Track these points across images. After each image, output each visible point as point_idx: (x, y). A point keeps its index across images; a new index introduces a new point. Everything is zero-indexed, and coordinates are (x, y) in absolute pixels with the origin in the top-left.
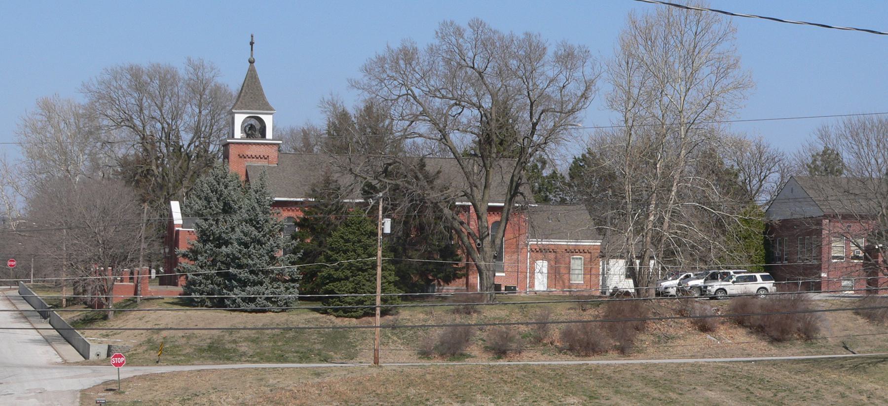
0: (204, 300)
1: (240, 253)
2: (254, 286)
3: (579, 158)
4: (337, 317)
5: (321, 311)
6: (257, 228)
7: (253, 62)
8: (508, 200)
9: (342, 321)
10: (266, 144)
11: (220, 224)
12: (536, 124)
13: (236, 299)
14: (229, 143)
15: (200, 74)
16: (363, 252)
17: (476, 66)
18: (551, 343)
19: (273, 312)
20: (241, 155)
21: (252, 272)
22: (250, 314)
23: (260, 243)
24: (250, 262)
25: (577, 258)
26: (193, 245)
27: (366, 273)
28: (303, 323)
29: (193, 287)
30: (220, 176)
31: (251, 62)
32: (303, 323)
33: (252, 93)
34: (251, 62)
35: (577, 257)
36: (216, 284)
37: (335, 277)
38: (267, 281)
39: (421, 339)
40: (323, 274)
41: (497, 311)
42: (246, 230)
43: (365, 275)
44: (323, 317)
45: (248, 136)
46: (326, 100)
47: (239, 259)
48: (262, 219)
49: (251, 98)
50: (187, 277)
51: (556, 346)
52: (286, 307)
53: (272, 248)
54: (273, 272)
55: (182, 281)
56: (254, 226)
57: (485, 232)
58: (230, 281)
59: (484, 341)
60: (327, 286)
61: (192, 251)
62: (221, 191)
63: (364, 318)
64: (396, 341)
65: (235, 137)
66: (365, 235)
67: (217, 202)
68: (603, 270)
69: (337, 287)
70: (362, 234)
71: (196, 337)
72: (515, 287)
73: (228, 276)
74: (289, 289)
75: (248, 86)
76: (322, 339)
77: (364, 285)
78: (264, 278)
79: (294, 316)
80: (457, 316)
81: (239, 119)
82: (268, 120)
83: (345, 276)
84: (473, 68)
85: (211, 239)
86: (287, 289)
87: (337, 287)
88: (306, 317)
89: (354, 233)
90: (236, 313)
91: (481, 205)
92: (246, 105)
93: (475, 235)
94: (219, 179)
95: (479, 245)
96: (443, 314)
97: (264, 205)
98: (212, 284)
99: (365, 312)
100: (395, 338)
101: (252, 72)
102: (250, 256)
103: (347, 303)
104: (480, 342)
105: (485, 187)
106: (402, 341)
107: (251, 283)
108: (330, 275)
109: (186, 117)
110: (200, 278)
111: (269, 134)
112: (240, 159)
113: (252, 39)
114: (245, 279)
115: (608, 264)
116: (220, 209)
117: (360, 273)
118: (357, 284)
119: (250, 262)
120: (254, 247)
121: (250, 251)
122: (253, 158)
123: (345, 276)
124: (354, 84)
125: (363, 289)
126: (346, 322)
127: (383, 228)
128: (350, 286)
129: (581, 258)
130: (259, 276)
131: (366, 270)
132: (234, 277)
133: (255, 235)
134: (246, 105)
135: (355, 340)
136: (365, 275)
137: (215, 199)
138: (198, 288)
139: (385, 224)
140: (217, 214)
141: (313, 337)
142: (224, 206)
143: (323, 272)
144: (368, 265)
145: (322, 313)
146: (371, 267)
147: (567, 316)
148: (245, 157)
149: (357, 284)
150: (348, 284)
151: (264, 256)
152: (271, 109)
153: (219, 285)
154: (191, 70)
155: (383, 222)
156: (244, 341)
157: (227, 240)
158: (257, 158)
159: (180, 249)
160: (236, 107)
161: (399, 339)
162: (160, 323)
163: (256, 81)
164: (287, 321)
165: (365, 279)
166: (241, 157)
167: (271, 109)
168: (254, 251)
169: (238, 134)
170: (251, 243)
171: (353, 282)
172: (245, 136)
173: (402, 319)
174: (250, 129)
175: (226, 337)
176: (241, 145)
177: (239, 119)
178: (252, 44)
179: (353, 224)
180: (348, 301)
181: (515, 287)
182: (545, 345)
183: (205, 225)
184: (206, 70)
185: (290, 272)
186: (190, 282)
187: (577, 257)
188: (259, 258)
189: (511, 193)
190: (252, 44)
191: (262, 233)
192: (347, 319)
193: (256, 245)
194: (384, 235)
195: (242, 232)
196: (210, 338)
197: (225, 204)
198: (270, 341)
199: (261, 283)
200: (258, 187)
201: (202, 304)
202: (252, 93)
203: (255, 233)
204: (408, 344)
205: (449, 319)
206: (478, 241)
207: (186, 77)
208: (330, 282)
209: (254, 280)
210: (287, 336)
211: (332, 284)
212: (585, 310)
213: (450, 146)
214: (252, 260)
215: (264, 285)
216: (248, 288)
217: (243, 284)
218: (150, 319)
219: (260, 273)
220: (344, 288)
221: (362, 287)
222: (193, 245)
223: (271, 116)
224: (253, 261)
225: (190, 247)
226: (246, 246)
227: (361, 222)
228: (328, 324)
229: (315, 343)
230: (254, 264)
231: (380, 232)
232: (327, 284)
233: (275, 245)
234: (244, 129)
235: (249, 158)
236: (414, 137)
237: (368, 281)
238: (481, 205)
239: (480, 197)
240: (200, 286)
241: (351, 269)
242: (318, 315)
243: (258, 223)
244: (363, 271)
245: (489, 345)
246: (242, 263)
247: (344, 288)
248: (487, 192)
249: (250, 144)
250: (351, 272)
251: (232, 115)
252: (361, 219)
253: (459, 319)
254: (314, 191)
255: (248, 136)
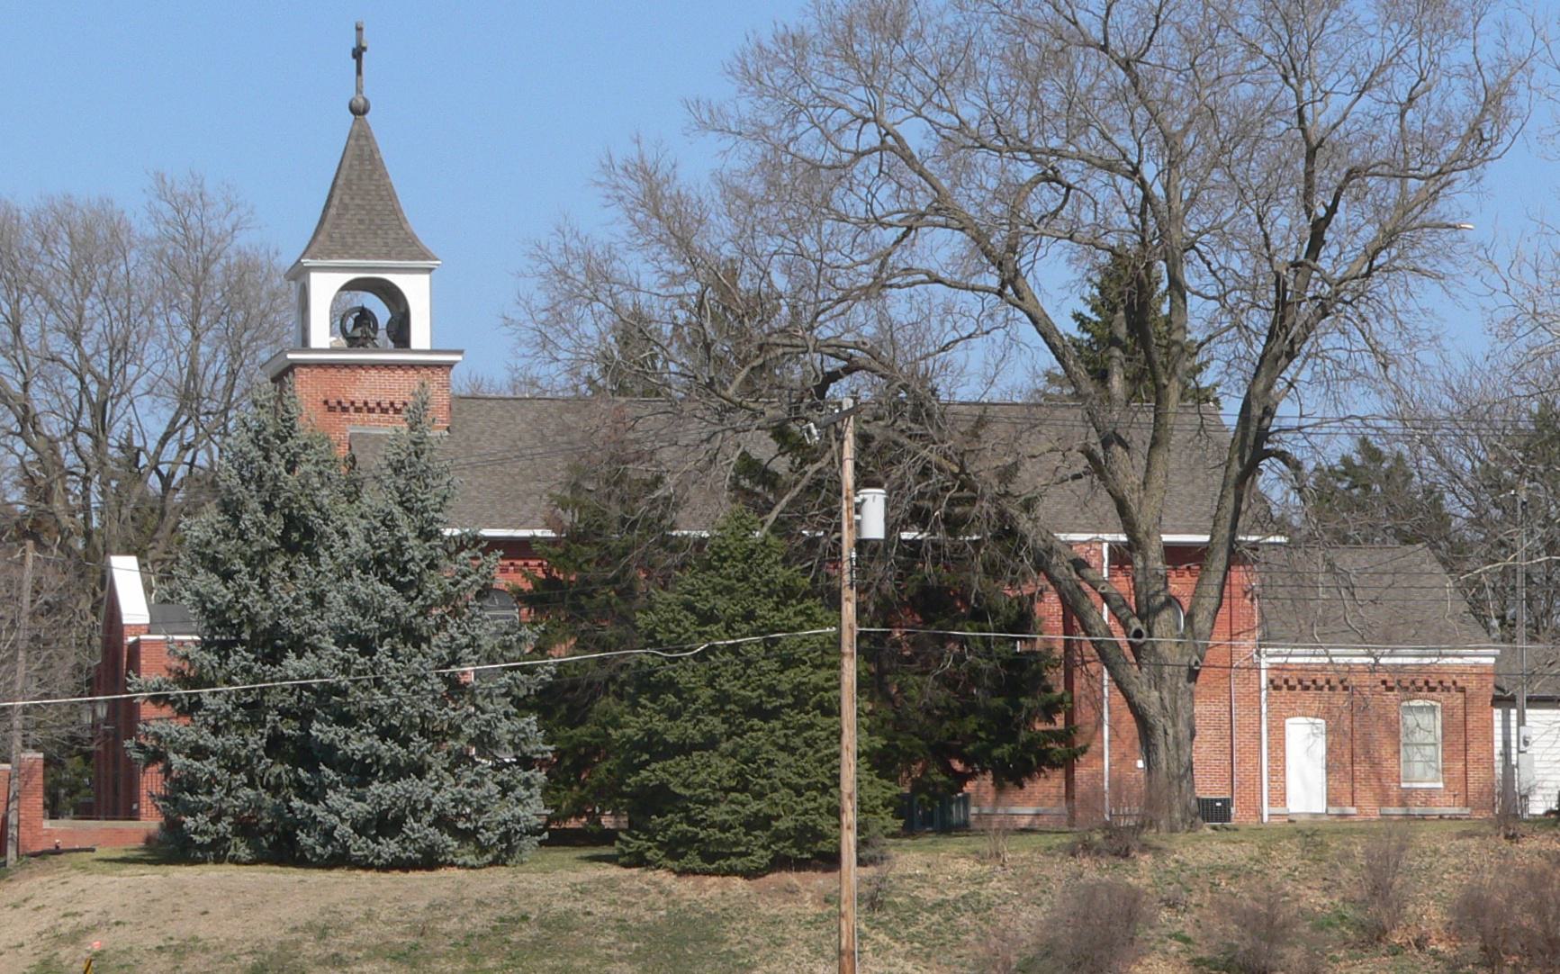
0: (225, 839)
1: (345, 672)
2: (395, 780)
3: (1331, 469)
4: (682, 873)
5: (621, 860)
6: (401, 588)
7: (365, 112)
8: (1231, 482)
9: (696, 886)
10: (413, 366)
11: (275, 584)
12: (1327, 220)
13: (335, 827)
14: (292, 366)
15: (193, 220)
16: (762, 650)
17: (1114, 42)
18: (1418, 946)
19: (464, 866)
20: (333, 402)
21: (385, 733)
22: (384, 875)
23: (414, 637)
24: (381, 699)
25: (1421, 708)
26: (186, 657)
27: (776, 724)
28: (565, 897)
29: (188, 797)
30: (271, 430)
31: (358, 111)
32: (565, 897)
33: (362, 207)
34: (358, 111)
35: (1421, 703)
36: (267, 787)
37: (670, 738)
38: (438, 761)
39: (971, 937)
40: (629, 731)
41: (1218, 846)
42: (362, 591)
43: (773, 731)
44: (632, 877)
45: (353, 342)
46: (618, 161)
47: (343, 693)
48: (418, 556)
49: (361, 222)
50: (168, 770)
51: (1435, 953)
52: (504, 851)
53: (453, 653)
54: (459, 729)
55: (151, 782)
56: (392, 582)
57: (1157, 593)
58: (313, 769)
59: (1187, 940)
60: (644, 773)
61: (183, 679)
62: (276, 477)
63: (770, 876)
64: (887, 948)
65: (314, 344)
66: (769, 595)
67: (261, 515)
68: (1506, 743)
69: (677, 774)
70: (757, 592)
71: (205, 950)
72: (1227, 803)
73: (308, 754)
74: (513, 789)
75: (349, 183)
76: (634, 945)
77: (770, 763)
78: (429, 752)
79: (533, 877)
80: (1086, 862)
81: (325, 288)
82: (415, 289)
83: (703, 734)
84: (1105, 48)
85: (246, 636)
86: (505, 789)
87: (677, 774)
88: (572, 877)
89: (730, 590)
90: (336, 874)
91: (1140, 503)
92: (344, 245)
93: (1125, 604)
94: (266, 441)
95: (1138, 634)
96: (1037, 857)
97: (425, 510)
98: (251, 784)
99: (776, 853)
100: (882, 938)
101: (363, 142)
102: (378, 683)
103: (712, 825)
104: (1175, 946)
105: (1155, 443)
106: (908, 946)
107: (386, 769)
108: (651, 733)
109: (151, 352)
110: (209, 766)
111: (420, 335)
112: (331, 417)
113: (359, 39)
114: (365, 757)
115: (1521, 721)
116: (273, 537)
117: (756, 722)
118: (746, 761)
119: (381, 699)
120: (393, 649)
121: (379, 663)
122: (371, 410)
123: (703, 734)
124: (706, 116)
125: (766, 777)
126: (709, 891)
127: (858, 523)
128: (724, 767)
129: (1433, 708)
130: (412, 745)
131: (775, 713)
132: (328, 753)
133: (394, 609)
134: (344, 245)
135: (746, 945)
136: (773, 731)
137: (254, 504)
138: (203, 798)
139: (867, 508)
140: (262, 553)
141: (602, 941)
142: (286, 531)
143: (627, 725)
144: (780, 695)
145: (626, 866)
146: (790, 700)
147: (1457, 856)
148: (345, 410)
149: (746, 761)
150: (715, 760)
151: (425, 677)
152: (425, 255)
153: (275, 789)
154: (167, 210)
155: (858, 500)
156: (369, 958)
157: (300, 638)
158: (384, 411)
159: (143, 675)
160: (314, 249)
161: (897, 940)
162: (79, 909)
163: (373, 171)
164: (510, 890)
165: (775, 744)
166: (331, 409)
167: (425, 255)
168: (392, 664)
169: (322, 334)
170: (383, 637)
171: (733, 754)
172: (343, 343)
173: (902, 878)
174: (358, 322)
175: (306, 945)
176: (333, 371)
177: (325, 288)
178: (358, 53)
179: (725, 559)
180: (718, 819)
181: (1227, 803)
182: (1396, 951)
183: (222, 593)
184: (210, 211)
185: (514, 733)
186: (178, 781)
187: (1421, 703)
188: (408, 687)
189: (1241, 458)
190: (358, 53)
191: (419, 602)
192: (714, 879)
193: (400, 646)
194: (861, 544)
195: (354, 602)
196: (253, 952)
197: (291, 522)
198: (458, 957)
199: (420, 771)
200: (404, 455)
201: (217, 852)
202: (362, 207)
203: (397, 601)
204: (928, 956)
205: (1059, 870)
206: (1136, 624)
207: (152, 231)
208: (656, 757)
209: (395, 760)
210: (514, 938)
211: (660, 765)
212: (1514, 836)
213: (1033, 310)
214: (388, 692)
215: (429, 776)
216: (376, 787)
217: (360, 772)
218: (47, 902)
219: (415, 735)
220: (704, 775)
221: (765, 770)
222: (186, 657)
223: (425, 278)
224: (390, 695)
225: (176, 664)
226: (366, 647)
227: (753, 551)
228: (650, 898)
229: (610, 959)
230: (393, 706)
231: (848, 538)
232: (644, 765)
233: (465, 640)
234: (339, 318)
235: (358, 410)
236: (914, 284)
237: (782, 748)
238: (1140, 503)
239: (1136, 478)
240: (210, 793)
241: (722, 709)
242: (613, 871)
243: (404, 571)
244: (766, 716)
245: (1205, 954)
246: (353, 709)
247: (704, 775)
248: (1159, 457)
249: (360, 365)
250: (724, 721)
251: (299, 275)
252: (750, 543)
253: (1092, 871)
254: (575, 487)
255: (353, 342)
